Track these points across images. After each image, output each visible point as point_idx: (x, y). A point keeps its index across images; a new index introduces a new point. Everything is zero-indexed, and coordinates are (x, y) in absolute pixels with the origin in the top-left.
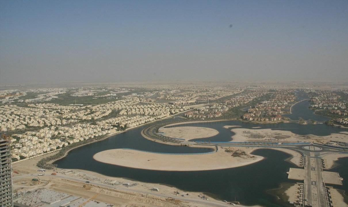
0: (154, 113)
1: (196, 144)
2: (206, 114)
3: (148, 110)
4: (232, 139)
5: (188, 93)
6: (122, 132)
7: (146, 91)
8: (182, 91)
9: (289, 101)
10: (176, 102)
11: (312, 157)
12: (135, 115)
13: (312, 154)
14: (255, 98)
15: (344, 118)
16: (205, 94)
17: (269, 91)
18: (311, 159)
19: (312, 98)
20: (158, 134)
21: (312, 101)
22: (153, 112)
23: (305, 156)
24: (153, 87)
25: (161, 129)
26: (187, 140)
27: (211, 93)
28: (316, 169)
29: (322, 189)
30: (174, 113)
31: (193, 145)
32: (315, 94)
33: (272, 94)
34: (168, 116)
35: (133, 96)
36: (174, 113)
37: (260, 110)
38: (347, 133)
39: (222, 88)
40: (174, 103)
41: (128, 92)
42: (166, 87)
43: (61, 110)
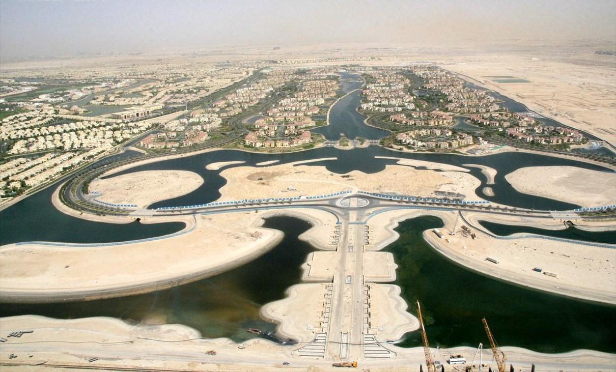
0: (81, 144)
1: (158, 213)
2: (180, 136)
3: (70, 138)
4: (218, 196)
5: (152, 85)
6: (18, 199)
7: (70, 86)
8: (139, 82)
9: (327, 97)
10: (126, 113)
11: (352, 223)
12: (41, 153)
13: (353, 216)
14: (271, 91)
15: (409, 132)
16: (182, 86)
17: (296, 73)
18: (350, 226)
19: (365, 88)
20: (86, 197)
21: (364, 93)
22: (80, 142)
23: (341, 223)
24: (86, 74)
25: (96, 186)
26: (140, 207)
27: (193, 83)
28: (355, 249)
29: (361, 290)
30: (120, 141)
31: (150, 218)
32: (370, 79)
33: (300, 80)
34: (108, 147)
35: (41, 102)
36: (120, 140)
37: (277, 119)
38: (615, 245)
39: (214, 70)
40: (122, 116)
41: (33, 91)
42: (110, 72)
43: (405, 173)
